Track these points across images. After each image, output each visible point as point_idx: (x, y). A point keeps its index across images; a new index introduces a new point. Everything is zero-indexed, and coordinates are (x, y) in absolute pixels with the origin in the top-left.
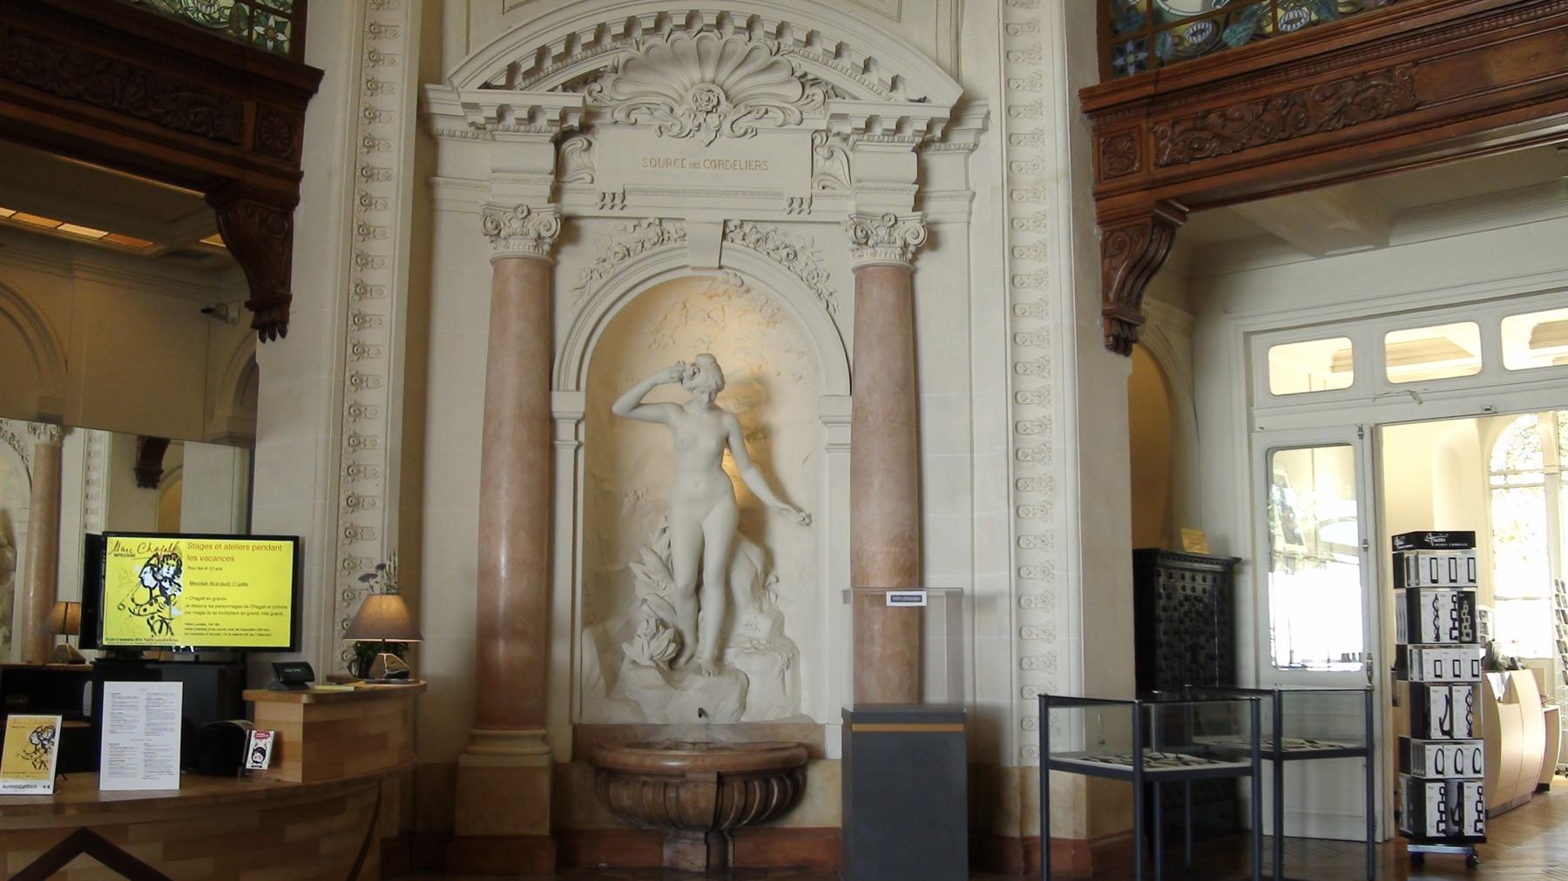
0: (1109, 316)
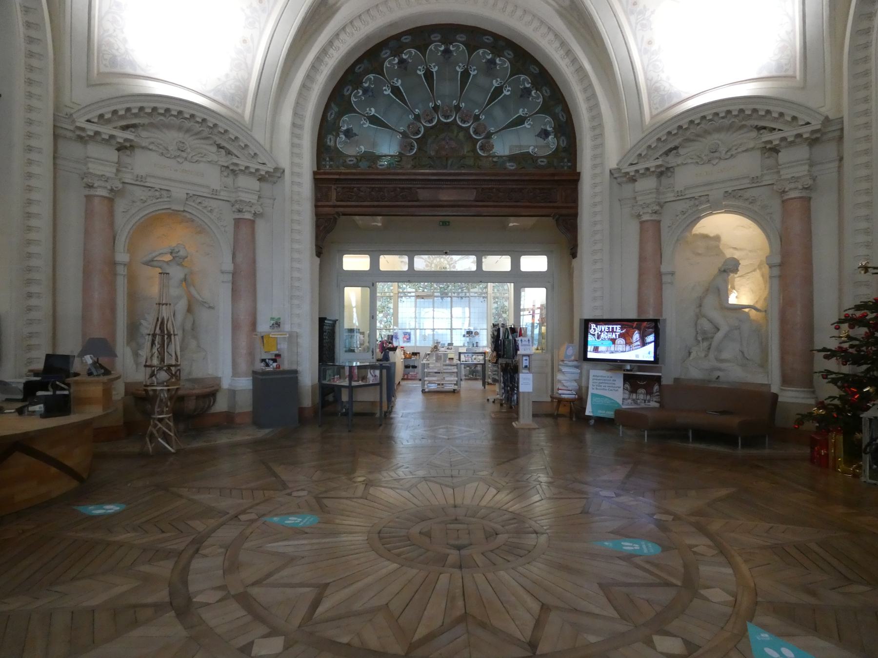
0: (316, 246)
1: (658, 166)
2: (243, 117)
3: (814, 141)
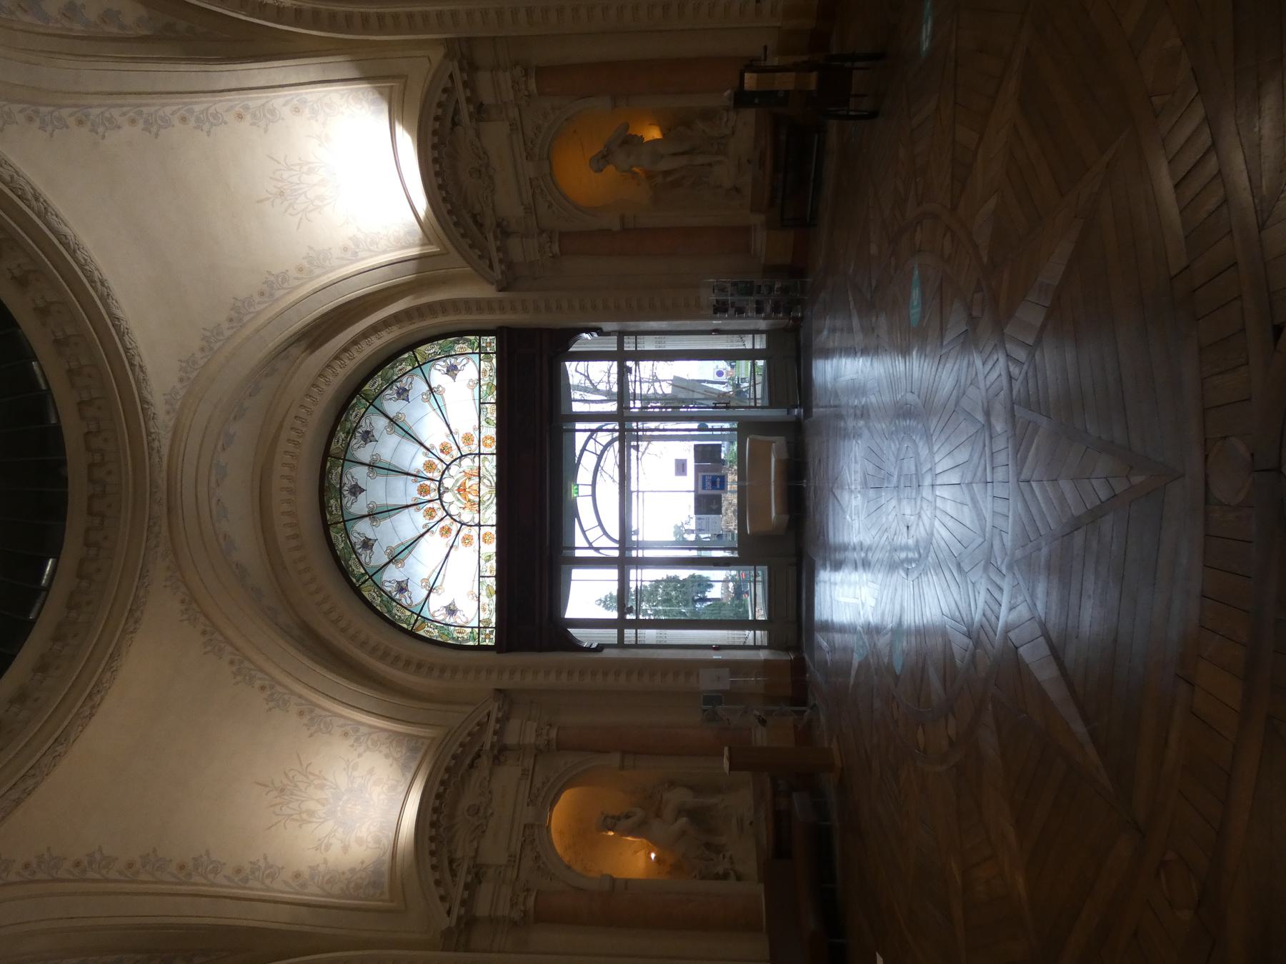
1: (496, 237)
2: (433, 739)
3: (470, 66)
